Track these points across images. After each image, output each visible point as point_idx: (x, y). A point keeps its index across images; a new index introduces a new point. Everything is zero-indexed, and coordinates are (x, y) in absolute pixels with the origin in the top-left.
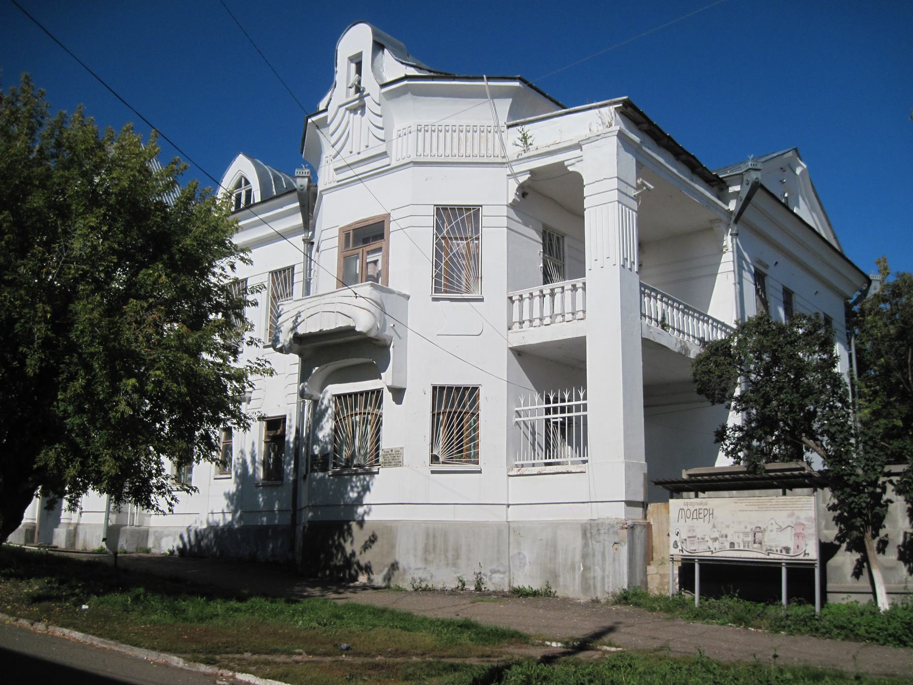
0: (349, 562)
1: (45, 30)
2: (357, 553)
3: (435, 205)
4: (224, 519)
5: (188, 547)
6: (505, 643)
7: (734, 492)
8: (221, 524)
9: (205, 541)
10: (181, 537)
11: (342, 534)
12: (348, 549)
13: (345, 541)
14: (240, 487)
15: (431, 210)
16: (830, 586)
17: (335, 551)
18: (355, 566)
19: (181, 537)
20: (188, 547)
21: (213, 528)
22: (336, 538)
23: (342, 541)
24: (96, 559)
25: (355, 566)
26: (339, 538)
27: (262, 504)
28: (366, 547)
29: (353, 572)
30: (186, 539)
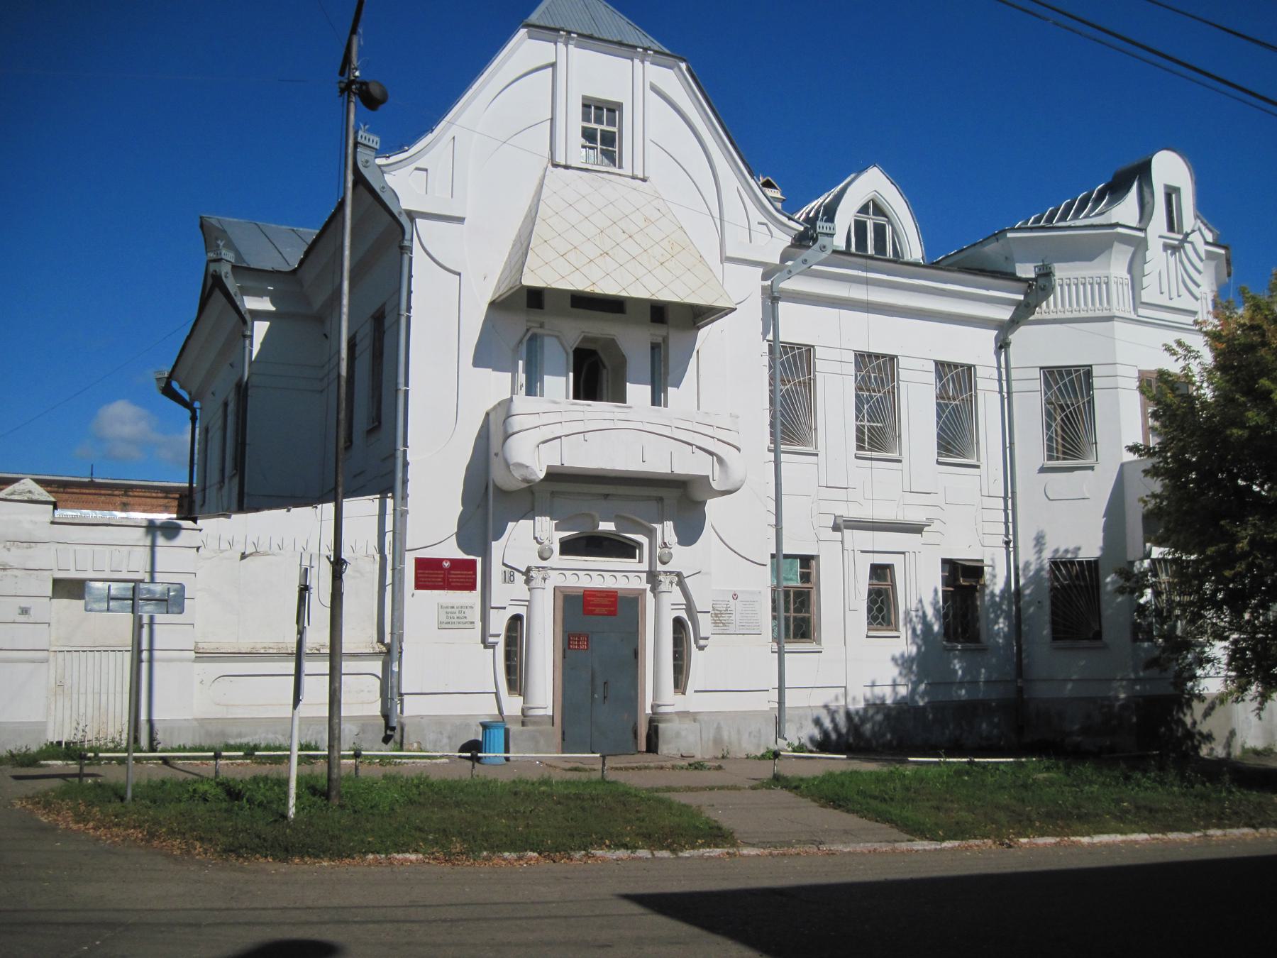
0: (1189, 735)
1: (265, 235)
2: (1198, 722)
3: (1041, 368)
4: (895, 693)
5: (834, 736)
6: (1233, 744)
7: (639, 691)
8: (889, 701)
9: (868, 726)
10: (817, 722)
11: (1180, 709)
12: (1188, 720)
13: (1185, 715)
14: (1098, 845)
15: (1037, 373)
16: (157, 645)
17: (1175, 727)
18: (1198, 737)
19: (817, 722)
20: (834, 736)
21: (876, 706)
22: (1174, 713)
23: (1182, 716)
24: (557, 776)
25: (1198, 737)
26: (1177, 712)
27: (960, 672)
28: (1207, 714)
29: (1196, 743)
30: (828, 724)
